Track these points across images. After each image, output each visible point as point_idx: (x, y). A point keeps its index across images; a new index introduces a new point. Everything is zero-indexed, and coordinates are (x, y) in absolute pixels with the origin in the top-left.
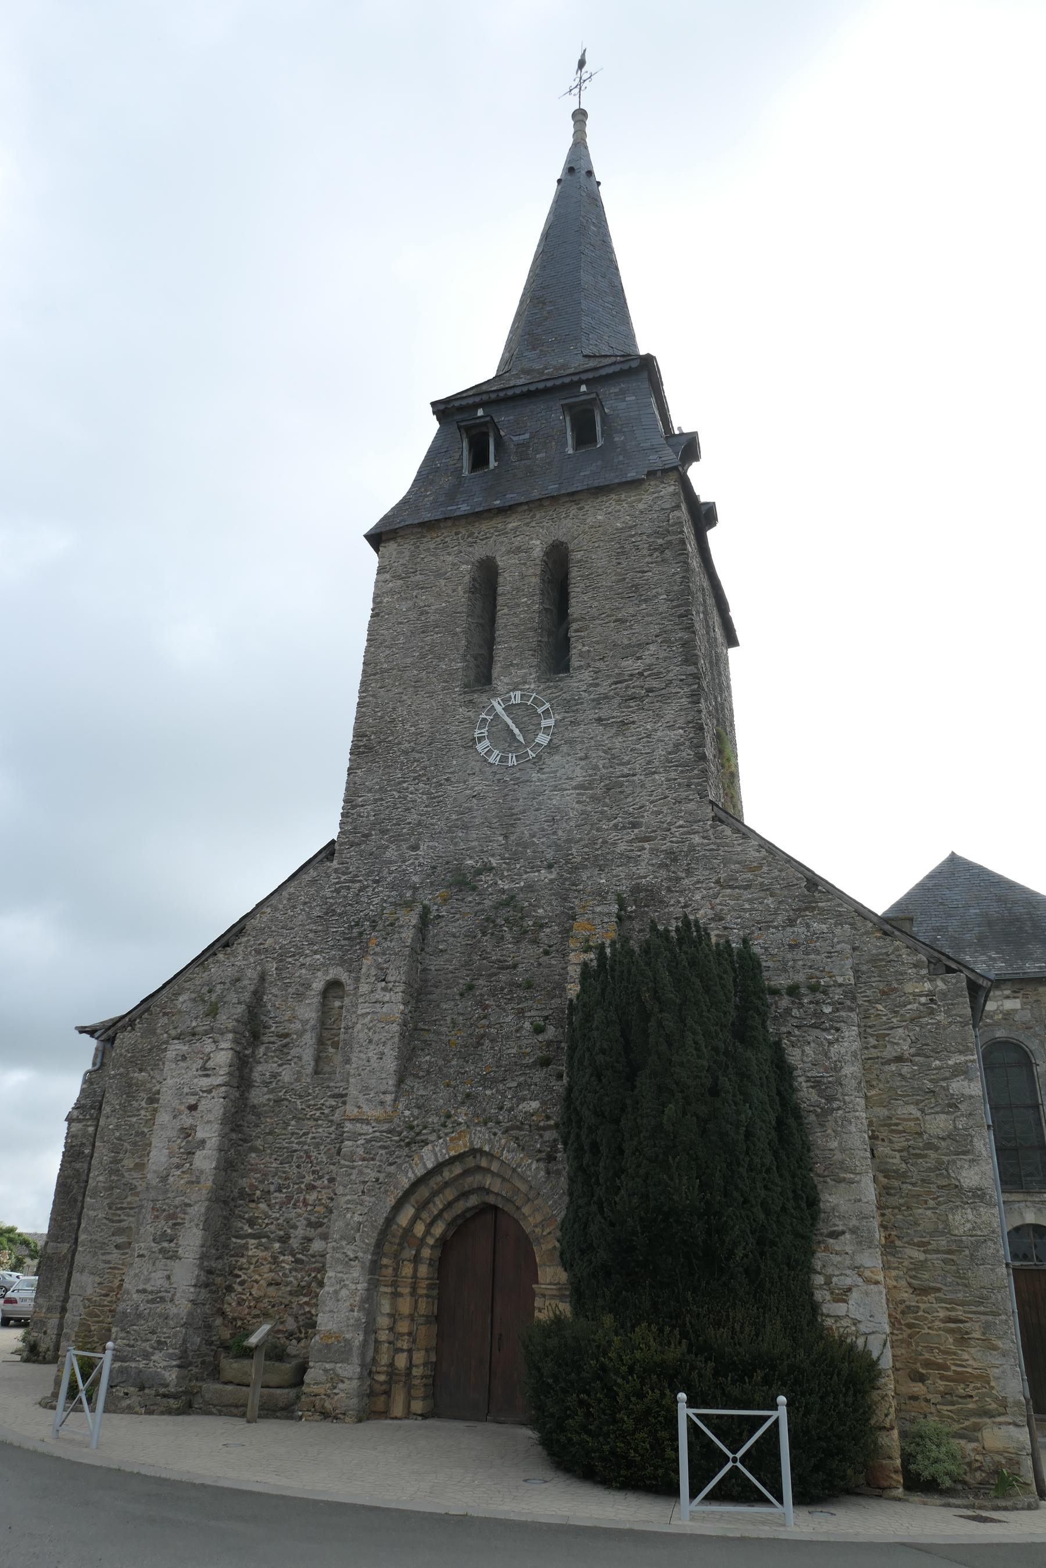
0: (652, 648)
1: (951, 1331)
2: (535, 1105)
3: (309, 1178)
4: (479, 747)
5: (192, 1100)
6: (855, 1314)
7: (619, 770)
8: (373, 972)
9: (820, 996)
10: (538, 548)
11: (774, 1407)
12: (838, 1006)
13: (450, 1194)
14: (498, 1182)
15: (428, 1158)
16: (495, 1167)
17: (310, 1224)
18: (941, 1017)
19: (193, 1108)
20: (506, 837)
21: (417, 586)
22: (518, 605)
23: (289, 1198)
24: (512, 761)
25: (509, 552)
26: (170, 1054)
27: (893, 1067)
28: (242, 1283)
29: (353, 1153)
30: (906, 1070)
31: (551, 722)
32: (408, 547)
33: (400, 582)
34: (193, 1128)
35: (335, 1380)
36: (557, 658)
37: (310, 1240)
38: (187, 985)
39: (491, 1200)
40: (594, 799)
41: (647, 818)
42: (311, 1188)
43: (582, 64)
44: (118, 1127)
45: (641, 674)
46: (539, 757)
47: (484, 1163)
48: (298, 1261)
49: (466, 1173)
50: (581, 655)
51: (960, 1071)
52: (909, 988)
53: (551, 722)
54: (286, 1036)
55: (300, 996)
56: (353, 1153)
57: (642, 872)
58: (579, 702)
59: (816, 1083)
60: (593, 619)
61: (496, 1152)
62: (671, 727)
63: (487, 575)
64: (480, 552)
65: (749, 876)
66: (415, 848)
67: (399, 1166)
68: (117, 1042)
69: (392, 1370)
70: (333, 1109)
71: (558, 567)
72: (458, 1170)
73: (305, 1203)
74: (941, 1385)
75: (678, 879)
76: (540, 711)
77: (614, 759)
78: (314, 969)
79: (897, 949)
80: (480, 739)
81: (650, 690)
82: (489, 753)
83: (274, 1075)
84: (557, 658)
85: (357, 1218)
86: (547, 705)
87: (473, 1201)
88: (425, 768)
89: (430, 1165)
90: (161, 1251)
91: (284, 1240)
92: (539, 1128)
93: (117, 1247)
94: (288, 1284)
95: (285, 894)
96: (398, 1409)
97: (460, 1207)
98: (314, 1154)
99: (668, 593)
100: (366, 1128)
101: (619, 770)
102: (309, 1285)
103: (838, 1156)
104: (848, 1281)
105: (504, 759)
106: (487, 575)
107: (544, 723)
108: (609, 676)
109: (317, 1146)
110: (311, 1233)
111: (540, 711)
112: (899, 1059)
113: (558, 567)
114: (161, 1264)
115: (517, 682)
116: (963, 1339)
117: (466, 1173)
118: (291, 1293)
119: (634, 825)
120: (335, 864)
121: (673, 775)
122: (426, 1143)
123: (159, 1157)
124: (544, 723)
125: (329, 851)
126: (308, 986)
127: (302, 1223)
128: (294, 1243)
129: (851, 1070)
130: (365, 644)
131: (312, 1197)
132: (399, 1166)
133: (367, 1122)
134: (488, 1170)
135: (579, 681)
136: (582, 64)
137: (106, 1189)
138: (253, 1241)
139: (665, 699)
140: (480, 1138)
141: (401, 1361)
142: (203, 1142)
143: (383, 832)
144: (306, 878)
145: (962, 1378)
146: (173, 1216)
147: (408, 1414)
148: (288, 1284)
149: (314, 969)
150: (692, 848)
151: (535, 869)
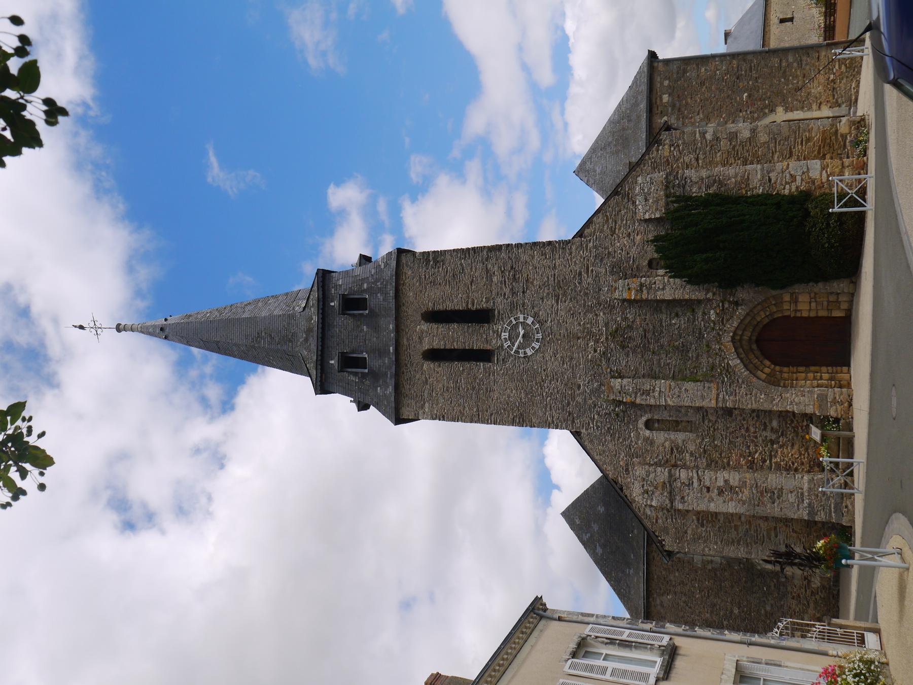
0: (489, 266)
1: (806, 144)
2: (712, 312)
3: (743, 431)
4: (529, 353)
5: (705, 490)
6: (800, 173)
7: (551, 282)
8: (644, 397)
9: (671, 185)
10: (424, 326)
11: (833, 180)
12: (676, 177)
13: (752, 356)
14: (746, 333)
15: (735, 362)
16: (740, 333)
17: (765, 429)
18: (680, 142)
19: (708, 489)
20: (579, 338)
21: (430, 395)
22: (453, 337)
23: (753, 441)
24: (540, 336)
25: (421, 342)
26: (680, 507)
27: (700, 162)
28: (793, 464)
29: (733, 401)
30: (701, 156)
31: (521, 317)
32: (406, 401)
33: (427, 404)
34: (719, 488)
35: (834, 402)
36: (483, 317)
37: (772, 429)
38: (642, 510)
39: (754, 338)
40: (565, 294)
41: (577, 268)
42: (747, 430)
43: (81, 327)
44: (716, 543)
45: (502, 272)
46: (539, 322)
47: (738, 338)
48: (782, 435)
49: (742, 347)
50: (487, 302)
51: (703, 135)
52: (667, 154)
53: (521, 317)
54: (672, 449)
55: (652, 443)
56: (733, 401)
57: (604, 271)
58: (512, 303)
59: (708, 187)
60: (468, 297)
61: (733, 329)
62: (533, 257)
63: (434, 355)
64: (417, 358)
65: (610, 221)
66: (579, 387)
67: (739, 377)
68: (671, 549)
69: (831, 379)
70: (710, 421)
71: (436, 317)
72: (741, 350)
73: (755, 432)
74: (827, 148)
75: (609, 253)
76: (514, 322)
77: (546, 285)
78: (638, 436)
79: (650, 158)
80: (525, 353)
81: (512, 268)
82: (533, 348)
83: (692, 454)
84: (483, 317)
85: (763, 396)
86: (512, 319)
87: (754, 346)
88: (536, 384)
89: (739, 361)
90: (779, 498)
91: (772, 442)
92: (723, 310)
93: (776, 536)
94: (793, 439)
95: (597, 458)
96: (846, 376)
97: (758, 353)
98: (731, 429)
99: (461, 259)
100: (721, 396)
101: (551, 282)
102: (793, 427)
103: (739, 179)
104: (788, 175)
105: (538, 340)
106: (434, 355)
107: (521, 320)
108: (501, 288)
109: (727, 428)
110: (769, 428)
111: (514, 322)
112: (697, 160)
113: (436, 317)
114: (784, 497)
115: (499, 336)
116: (809, 140)
117: (742, 347)
118: (797, 436)
119: (580, 274)
120: (583, 431)
121: (557, 256)
122: (728, 364)
123: (731, 508)
124: (521, 320)
125: (577, 435)
126: (646, 439)
127: (764, 433)
128: (774, 437)
129: (704, 173)
130: (460, 423)
131: (752, 429)
132: (739, 377)
133: (718, 395)
134: (742, 335)
135: (500, 304)
136: (81, 327)
137: (747, 546)
138: (773, 460)
139: (518, 259)
140: (727, 339)
141: (826, 376)
142: (726, 481)
143: (569, 404)
144: (589, 446)
145: (824, 140)
146: (762, 493)
147: (849, 372)
148: (793, 439)
149: (638, 436)
150: (595, 247)
151: (597, 322)
